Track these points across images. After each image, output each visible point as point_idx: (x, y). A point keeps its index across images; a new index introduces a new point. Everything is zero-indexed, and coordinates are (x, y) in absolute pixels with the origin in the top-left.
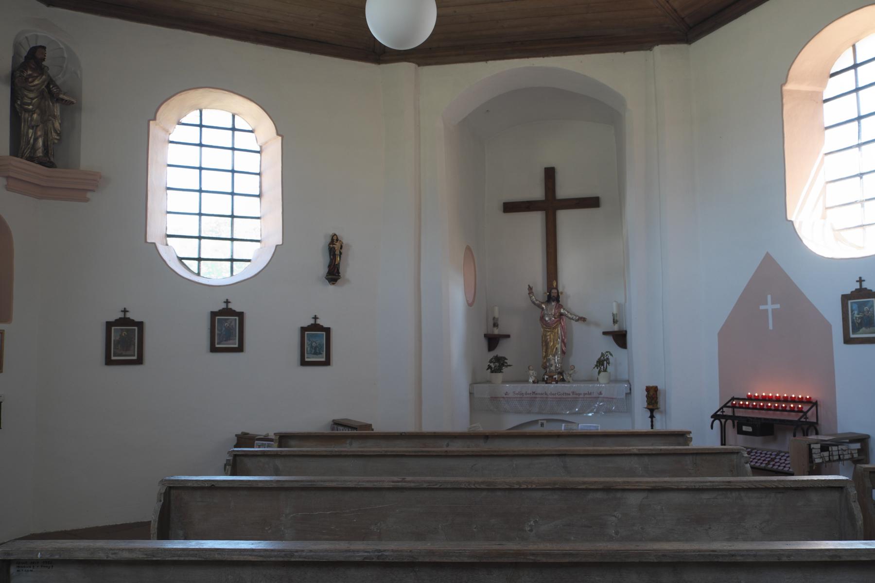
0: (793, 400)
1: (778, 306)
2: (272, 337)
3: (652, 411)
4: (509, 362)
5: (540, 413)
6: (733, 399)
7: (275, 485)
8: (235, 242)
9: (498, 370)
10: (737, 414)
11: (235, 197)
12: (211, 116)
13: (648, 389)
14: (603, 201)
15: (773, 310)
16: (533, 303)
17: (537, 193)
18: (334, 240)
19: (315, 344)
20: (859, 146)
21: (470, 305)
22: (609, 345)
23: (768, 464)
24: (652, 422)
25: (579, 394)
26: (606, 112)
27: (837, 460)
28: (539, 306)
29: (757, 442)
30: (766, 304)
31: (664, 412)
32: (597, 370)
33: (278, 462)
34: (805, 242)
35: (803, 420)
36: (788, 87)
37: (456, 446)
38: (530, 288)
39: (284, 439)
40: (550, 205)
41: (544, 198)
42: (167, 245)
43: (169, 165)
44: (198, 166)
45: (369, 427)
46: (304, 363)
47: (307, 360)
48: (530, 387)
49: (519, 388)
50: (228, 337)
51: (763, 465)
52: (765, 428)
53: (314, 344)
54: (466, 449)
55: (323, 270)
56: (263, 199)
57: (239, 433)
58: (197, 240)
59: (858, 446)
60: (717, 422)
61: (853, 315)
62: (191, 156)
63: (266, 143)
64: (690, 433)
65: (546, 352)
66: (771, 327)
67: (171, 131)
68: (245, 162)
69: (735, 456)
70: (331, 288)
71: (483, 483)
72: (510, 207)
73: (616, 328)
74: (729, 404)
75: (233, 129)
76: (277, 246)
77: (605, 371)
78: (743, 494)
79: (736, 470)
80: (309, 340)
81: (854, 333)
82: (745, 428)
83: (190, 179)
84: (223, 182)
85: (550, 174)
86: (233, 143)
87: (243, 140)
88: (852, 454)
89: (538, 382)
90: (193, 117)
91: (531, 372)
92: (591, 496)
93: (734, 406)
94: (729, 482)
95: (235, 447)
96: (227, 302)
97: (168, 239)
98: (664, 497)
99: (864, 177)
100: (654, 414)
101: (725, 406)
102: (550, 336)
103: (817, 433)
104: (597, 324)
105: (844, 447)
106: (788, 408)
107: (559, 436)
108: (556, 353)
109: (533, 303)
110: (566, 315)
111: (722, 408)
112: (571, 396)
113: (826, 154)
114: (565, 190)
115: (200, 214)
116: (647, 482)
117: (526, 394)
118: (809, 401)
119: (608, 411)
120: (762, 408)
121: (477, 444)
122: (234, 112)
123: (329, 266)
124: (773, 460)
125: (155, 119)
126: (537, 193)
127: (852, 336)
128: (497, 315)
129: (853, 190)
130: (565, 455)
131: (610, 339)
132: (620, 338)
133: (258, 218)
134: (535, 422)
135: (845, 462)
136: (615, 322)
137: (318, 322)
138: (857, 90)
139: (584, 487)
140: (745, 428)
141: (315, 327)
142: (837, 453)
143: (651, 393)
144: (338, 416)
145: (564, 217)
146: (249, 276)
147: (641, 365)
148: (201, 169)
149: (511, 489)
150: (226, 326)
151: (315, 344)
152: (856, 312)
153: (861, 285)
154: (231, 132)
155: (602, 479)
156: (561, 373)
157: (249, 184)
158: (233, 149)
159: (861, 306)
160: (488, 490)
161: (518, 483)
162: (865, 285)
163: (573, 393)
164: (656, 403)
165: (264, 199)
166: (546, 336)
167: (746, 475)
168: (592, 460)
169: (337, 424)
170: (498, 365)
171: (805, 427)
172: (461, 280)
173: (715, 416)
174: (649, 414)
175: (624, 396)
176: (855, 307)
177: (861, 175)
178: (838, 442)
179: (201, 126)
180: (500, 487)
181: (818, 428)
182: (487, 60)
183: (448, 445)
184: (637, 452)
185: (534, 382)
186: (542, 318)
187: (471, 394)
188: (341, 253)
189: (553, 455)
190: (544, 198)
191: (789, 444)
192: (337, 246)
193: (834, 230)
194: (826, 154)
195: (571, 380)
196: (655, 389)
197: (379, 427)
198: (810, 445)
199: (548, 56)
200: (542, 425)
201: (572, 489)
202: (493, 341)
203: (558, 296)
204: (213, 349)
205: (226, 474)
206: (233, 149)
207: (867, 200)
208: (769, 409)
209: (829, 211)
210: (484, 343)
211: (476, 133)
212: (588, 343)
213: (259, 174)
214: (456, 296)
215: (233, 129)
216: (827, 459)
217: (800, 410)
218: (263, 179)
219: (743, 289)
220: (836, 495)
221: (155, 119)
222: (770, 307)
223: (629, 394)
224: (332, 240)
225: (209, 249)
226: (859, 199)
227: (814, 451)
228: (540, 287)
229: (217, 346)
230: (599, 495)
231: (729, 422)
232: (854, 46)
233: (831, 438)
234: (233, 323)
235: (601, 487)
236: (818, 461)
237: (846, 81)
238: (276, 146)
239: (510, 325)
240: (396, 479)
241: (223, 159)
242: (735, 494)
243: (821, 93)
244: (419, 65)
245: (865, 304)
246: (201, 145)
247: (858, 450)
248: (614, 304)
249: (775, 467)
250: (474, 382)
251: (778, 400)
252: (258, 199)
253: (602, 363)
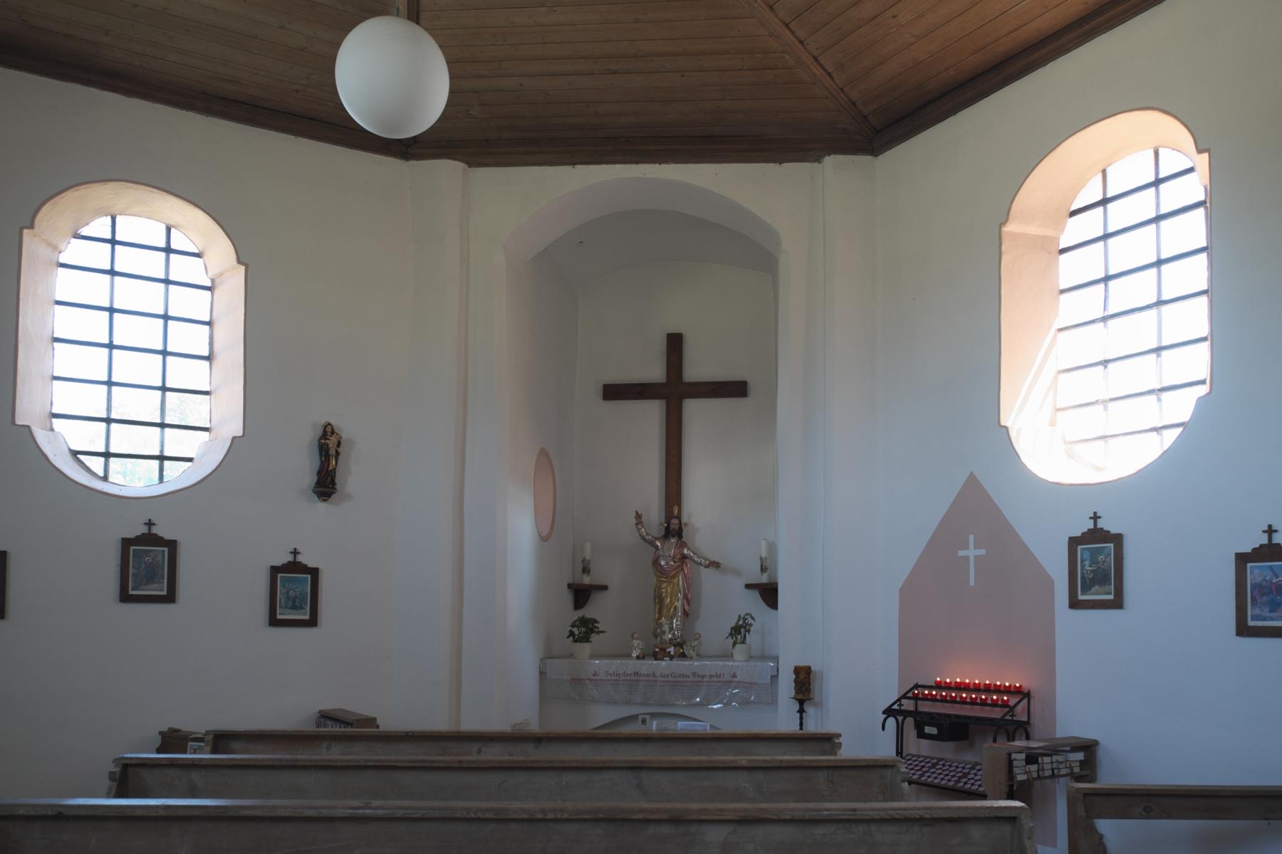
0: (998, 690)
1: (982, 552)
2: (220, 582)
3: (801, 702)
4: (601, 627)
5: (644, 704)
6: (916, 686)
7: (162, 813)
8: (167, 430)
9: (585, 638)
10: (920, 709)
11: (169, 358)
12: (129, 228)
13: (797, 670)
14: (752, 388)
15: (976, 557)
16: (643, 538)
17: (655, 372)
18: (328, 431)
19: (294, 593)
20: (1104, 319)
21: (544, 538)
22: (752, 604)
23: (958, 781)
24: (801, 718)
25: (704, 676)
26: (753, 253)
27: (1049, 777)
28: (652, 544)
29: (946, 750)
30: (967, 548)
31: (819, 705)
32: (731, 641)
33: (196, 776)
34: (1025, 459)
35: (1008, 717)
36: (1009, 228)
37: (492, 754)
38: (638, 516)
39: (221, 740)
40: (673, 390)
41: (664, 380)
42: (52, 430)
43: (58, 303)
44: (107, 305)
45: (371, 722)
46: (274, 622)
47: (279, 617)
48: (631, 665)
49: (616, 665)
50: (151, 575)
51: (951, 783)
52: (956, 730)
53: (292, 593)
54: (506, 758)
55: (308, 477)
56: (216, 364)
57: (165, 729)
58: (104, 425)
59: (1080, 756)
60: (891, 721)
61: (1083, 567)
62: (96, 289)
63: (221, 274)
64: (839, 736)
65: (660, 613)
66: (972, 583)
67: (62, 247)
68: (182, 302)
69: (888, 772)
70: (322, 506)
71: (488, 810)
72: (614, 392)
73: (764, 579)
74: (910, 695)
75: (168, 250)
76: (234, 438)
77: (743, 642)
78: (874, 827)
79: (890, 793)
80: (284, 586)
81: (1083, 592)
82: (928, 730)
83: (95, 325)
84: (150, 333)
85: (675, 343)
86: (167, 273)
87: (182, 268)
88: (1071, 768)
89: (643, 658)
90: (100, 227)
91: (636, 642)
92: (652, 829)
93: (916, 698)
94: (854, 810)
95: (159, 751)
96: (150, 524)
97: (54, 420)
98: (760, 831)
99: (1110, 366)
100: (805, 707)
101: (904, 696)
102: (667, 589)
103: (1028, 738)
105: (1060, 758)
106: (989, 701)
107: (647, 739)
108: (675, 614)
109: (643, 538)
110: (691, 558)
111: (899, 700)
112: (691, 678)
113: (1060, 330)
114: (694, 371)
115: (110, 383)
116: (734, 810)
117: (625, 674)
118: (1018, 691)
119: (745, 703)
120: (953, 701)
121: (519, 751)
122: (170, 222)
123: (319, 473)
124: (965, 775)
125: (31, 226)
126: (655, 372)
127: (1081, 597)
128: (588, 557)
129: (1094, 384)
130: (640, 768)
131: (755, 594)
132: (769, 594)
134: (633, 718)
135: (1061, 780)
136: (763, 569)
138: (1106, 237)
139: (640, 816)
140: (928, 730)
141: (295, 567)
142: (1049, 766)
143: (802, 677)
144: (328, 705)
145: (693, 409)
146: (187, 484)
147: (790, 636)
148: (112, 310)
149: (532, 821)
150: (148, 559)
151: (294, 593)
152: (1087, 563)
153: (1095, 524)
154: (163, 255)
155: (669, 806)
156: (680, 645)
157: (196, 340)
158: (167, 282)
159: (1094, 553)
160: (498, 820)
161: (543, 811)
162: (1101, 524)
163: (694, 674)
164: (809, 690)
165: (217, 363)
166: (660, 589)
167: (901, 799)
168: (680, 776)
169: (325, 716)
170: (585, 630)
171: (1011, 728)
172: (529, 501)
173: (889, 712)
174: (797, 708)
175: (768, 680)
176: (1087, 555)
177: (1105, 363)
178: (1053, 750)
179: (113, 242)
180: (514, 816)
181: (1029, 729)
182: (574, 164)
183: (479, 751)
184: (746, 764)
185: (638, 657)
186: (656, 562)
187: (542, 673)
188: (338, 454)
189: (622, 768)
190: (664, 380)
191: (987, 752)
192: (332, 442)
193: (1065, 442)
194: (1060, 330)
195: (694, 654)
196: (808, 670)
197: (389, 723)
198: (1010, 755)
199: (666, 162)
200: (644, 721)
201: (624, 820)
202: (581, 594)
203: (681, 529)
204: (125, 597)
205: (108, 796)
206: (167, 282)
207: (1112, 400)
208: (963, 702)
209: (1059, 414)
210: (568, 598)
211: (561, 275)
212: (724, 600)
213: (209, 323)
214: (520, 524)
215: (168, 250)
216: (1035, 775)
217: (1005, 704)
218: (216, 331)
219: (934, 527)
220: (1006, 829)
221: (31, 226)
222: (971, 553)
223: (775, 677)
224: (325, 433)
225: (123, 439)
226: (1101, 398)
227: (1015, 763)
229: (131, 592)
230: (665, 829)
231: (910, 720)
232: (1104, 172)
233: (1041, 744)
234: (159, 558)
235: (666, 816)
236: (1021, 777)
237: (1090, 224)
238: (235, 281)
239: (608, 571)
240: (355, 803)
241: (151, 298)
242: (861, 828)
243: (1057, 240)
244: (470, 165)
245: (1099, 551)
246: (112, 272)
247: (1081, 762)
248: (763, 543)
249: (968, 786)
250: (548, 656)
251: (977, 688)
252: (206, 363)
253: (740, 630)
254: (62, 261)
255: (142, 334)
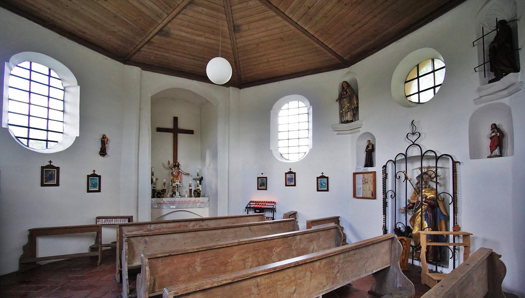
2: (72, 178)
12: (36, 66)
17: (170, 126)
40: (176, 130)
50: (51, 178)
70: (101, 158)
85: (176, 119)
90: (26, 64)
104: (191, 176)
114: (181, 125)
118: (274, 202)
122: (50, 68)
126: (170, 126)
133: (9, 112)
136: (198, 175)
137: (95, 173)
150: (50, 175)
192: (106, 140)
224: (103, 138)
228: (172, 162)
254: (12, 73)
255: (43, 101)
